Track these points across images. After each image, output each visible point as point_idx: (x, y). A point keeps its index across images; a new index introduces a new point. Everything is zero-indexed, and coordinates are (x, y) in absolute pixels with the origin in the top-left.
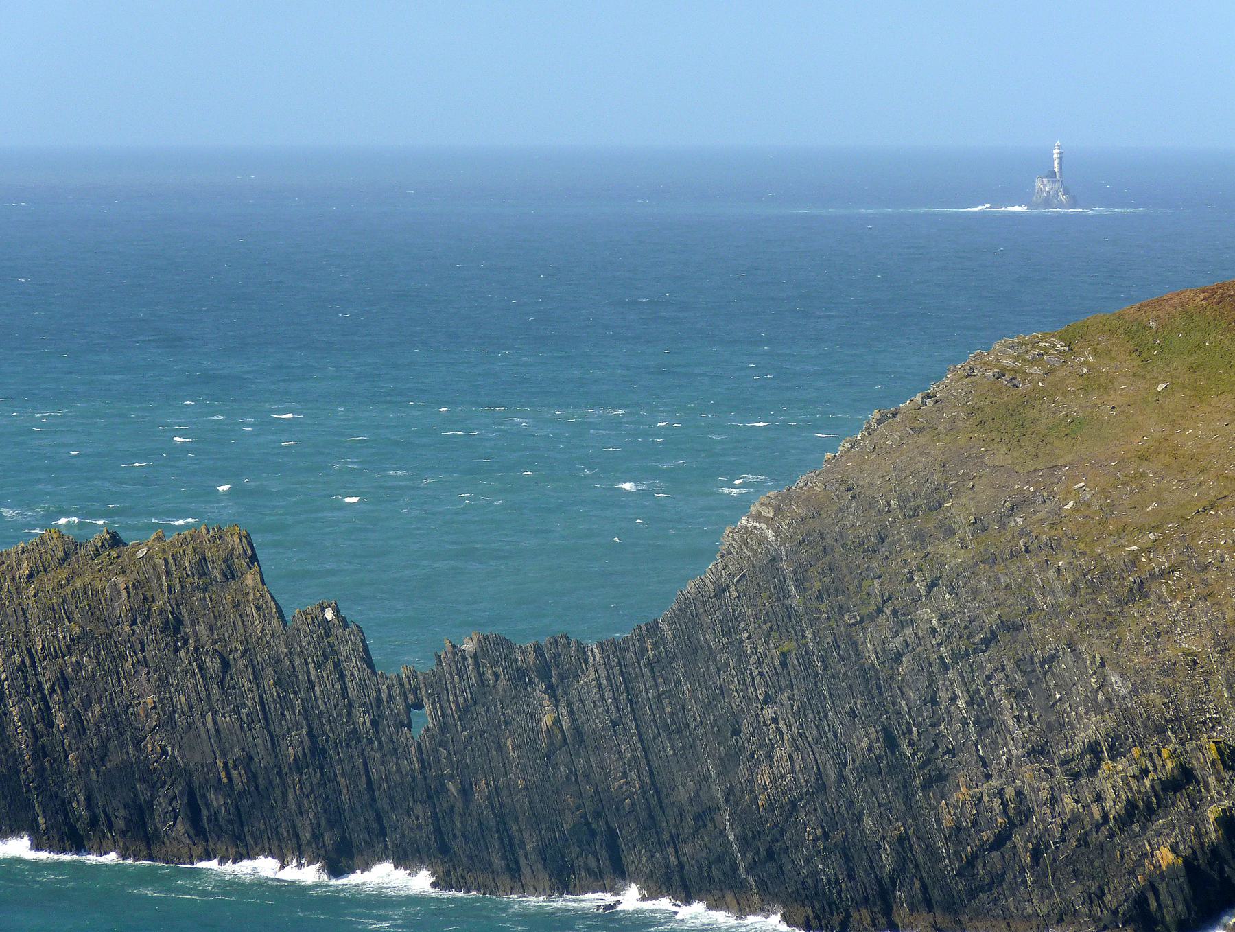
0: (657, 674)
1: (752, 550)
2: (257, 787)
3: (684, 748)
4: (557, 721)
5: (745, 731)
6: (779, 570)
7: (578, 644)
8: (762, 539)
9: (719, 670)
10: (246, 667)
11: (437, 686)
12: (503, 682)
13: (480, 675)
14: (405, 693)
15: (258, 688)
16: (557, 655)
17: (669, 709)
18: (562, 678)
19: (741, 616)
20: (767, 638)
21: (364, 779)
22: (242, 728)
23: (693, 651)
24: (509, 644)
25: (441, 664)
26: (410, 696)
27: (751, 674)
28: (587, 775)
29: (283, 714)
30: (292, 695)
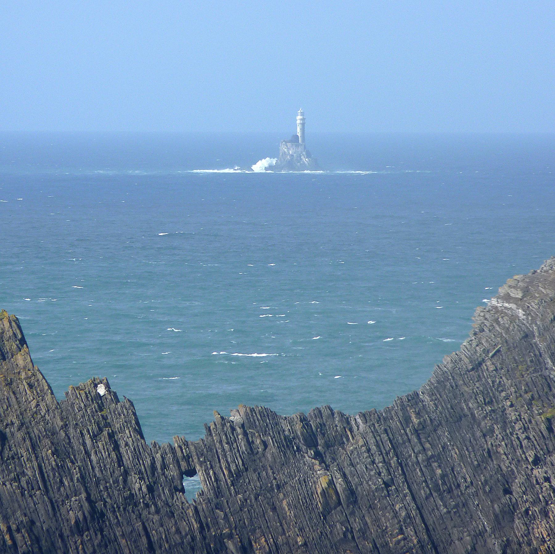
0: (423, 440)
1: (504, 328)
2: (40, 548)
3: (457, 506)
4: (331, 483)
5: (516, 488)
6: (532, 347)
7: (342, 415)
8: (513, 318)
9: (484, 436)
10: (24, 439)
11: (208, 454)
12: (272, 449)
13: (250, 444)
14: (178, 461)
15: (37, 457)
16: (322, 426)
17: (439, 472)
18: (328, 445)
19: (501, 387)
20: (530, 404)
21: (144, 540)
22: (23, 494)
23: (457, 418)
24: (274, 415)
25: (211, 435)
26: (183, 464)
27: (518, 438)
28: (363, 532)
29: (61, 482)
30: (70, 464)
